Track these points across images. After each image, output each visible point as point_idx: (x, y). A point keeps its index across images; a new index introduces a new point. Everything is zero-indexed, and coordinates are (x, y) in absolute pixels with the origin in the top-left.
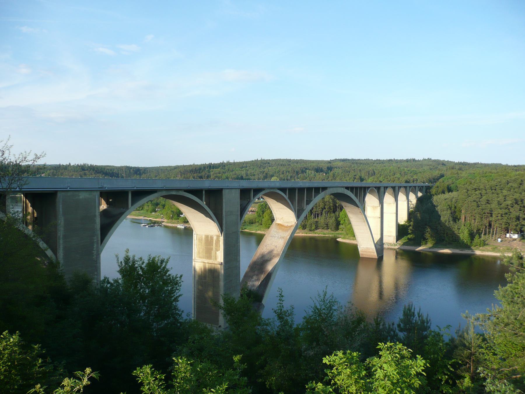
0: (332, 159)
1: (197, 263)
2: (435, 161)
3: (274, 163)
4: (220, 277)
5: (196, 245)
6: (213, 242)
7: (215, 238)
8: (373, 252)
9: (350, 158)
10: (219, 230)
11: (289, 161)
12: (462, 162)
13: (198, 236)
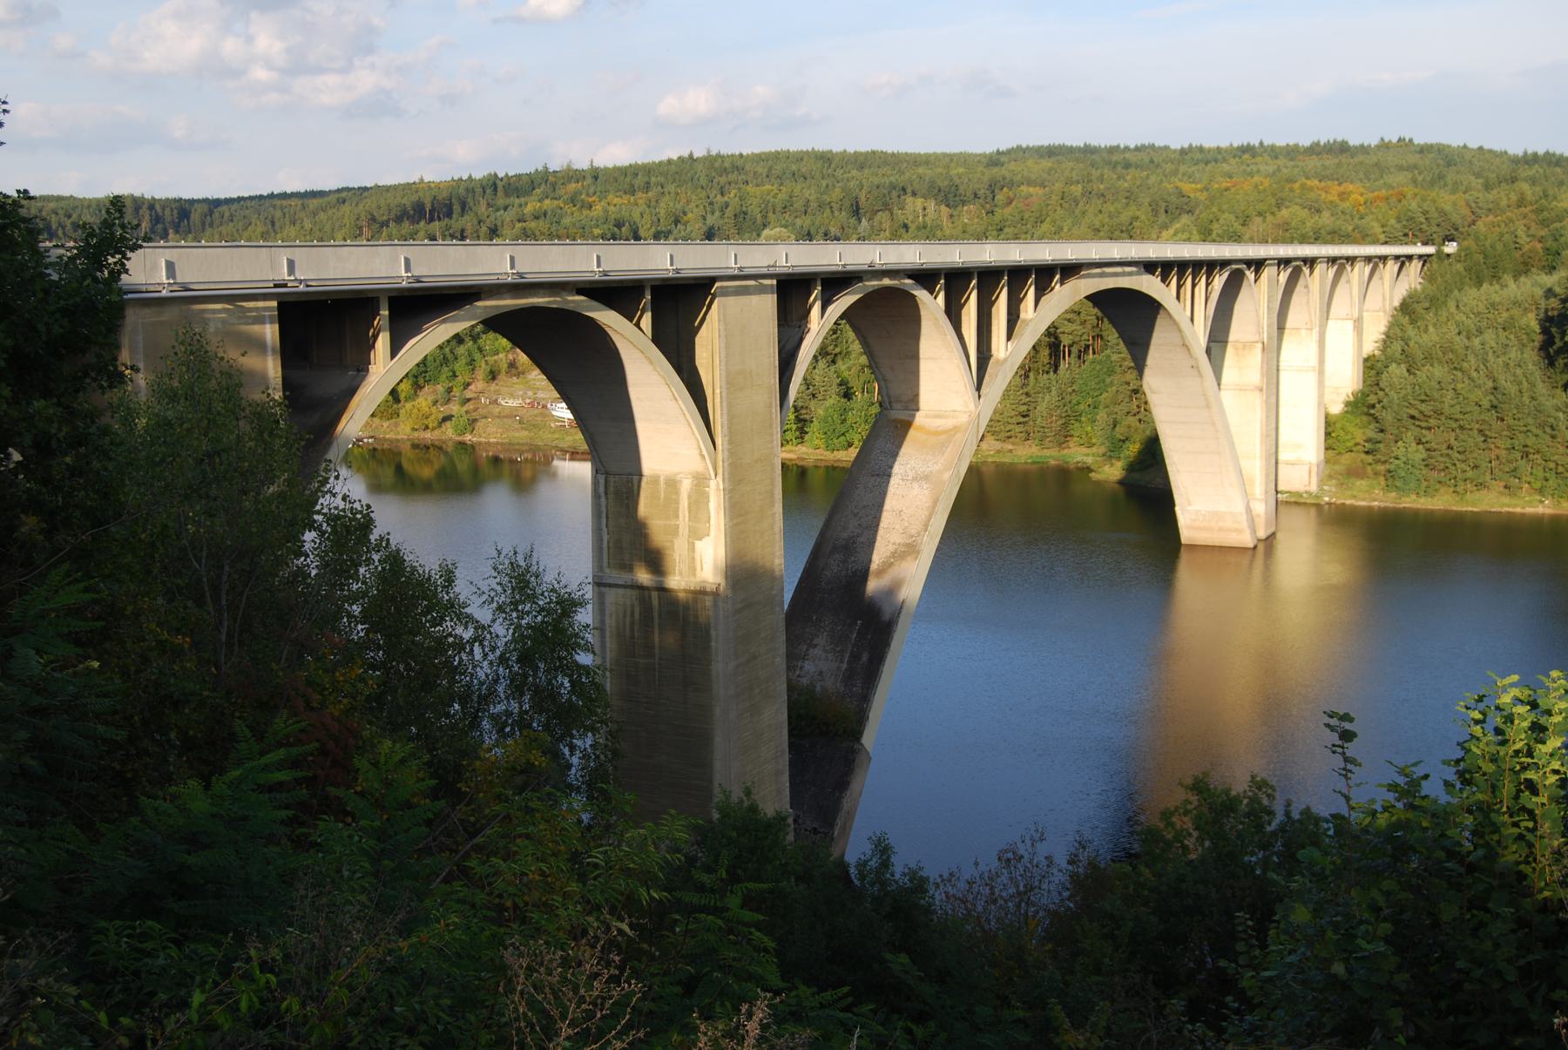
0: (1003, 148)
1: (614, 591)
2: (1424, 150)
3: (762, 169)
4: (713, 644)
5: (604, 515)
6: (677, 502)
7: (686, 485)
8: (1239, 531)
9: (1077, 141)
10: (705, 453)
11: (825, 158)
12: (1541, 152)
13: (612, 479)
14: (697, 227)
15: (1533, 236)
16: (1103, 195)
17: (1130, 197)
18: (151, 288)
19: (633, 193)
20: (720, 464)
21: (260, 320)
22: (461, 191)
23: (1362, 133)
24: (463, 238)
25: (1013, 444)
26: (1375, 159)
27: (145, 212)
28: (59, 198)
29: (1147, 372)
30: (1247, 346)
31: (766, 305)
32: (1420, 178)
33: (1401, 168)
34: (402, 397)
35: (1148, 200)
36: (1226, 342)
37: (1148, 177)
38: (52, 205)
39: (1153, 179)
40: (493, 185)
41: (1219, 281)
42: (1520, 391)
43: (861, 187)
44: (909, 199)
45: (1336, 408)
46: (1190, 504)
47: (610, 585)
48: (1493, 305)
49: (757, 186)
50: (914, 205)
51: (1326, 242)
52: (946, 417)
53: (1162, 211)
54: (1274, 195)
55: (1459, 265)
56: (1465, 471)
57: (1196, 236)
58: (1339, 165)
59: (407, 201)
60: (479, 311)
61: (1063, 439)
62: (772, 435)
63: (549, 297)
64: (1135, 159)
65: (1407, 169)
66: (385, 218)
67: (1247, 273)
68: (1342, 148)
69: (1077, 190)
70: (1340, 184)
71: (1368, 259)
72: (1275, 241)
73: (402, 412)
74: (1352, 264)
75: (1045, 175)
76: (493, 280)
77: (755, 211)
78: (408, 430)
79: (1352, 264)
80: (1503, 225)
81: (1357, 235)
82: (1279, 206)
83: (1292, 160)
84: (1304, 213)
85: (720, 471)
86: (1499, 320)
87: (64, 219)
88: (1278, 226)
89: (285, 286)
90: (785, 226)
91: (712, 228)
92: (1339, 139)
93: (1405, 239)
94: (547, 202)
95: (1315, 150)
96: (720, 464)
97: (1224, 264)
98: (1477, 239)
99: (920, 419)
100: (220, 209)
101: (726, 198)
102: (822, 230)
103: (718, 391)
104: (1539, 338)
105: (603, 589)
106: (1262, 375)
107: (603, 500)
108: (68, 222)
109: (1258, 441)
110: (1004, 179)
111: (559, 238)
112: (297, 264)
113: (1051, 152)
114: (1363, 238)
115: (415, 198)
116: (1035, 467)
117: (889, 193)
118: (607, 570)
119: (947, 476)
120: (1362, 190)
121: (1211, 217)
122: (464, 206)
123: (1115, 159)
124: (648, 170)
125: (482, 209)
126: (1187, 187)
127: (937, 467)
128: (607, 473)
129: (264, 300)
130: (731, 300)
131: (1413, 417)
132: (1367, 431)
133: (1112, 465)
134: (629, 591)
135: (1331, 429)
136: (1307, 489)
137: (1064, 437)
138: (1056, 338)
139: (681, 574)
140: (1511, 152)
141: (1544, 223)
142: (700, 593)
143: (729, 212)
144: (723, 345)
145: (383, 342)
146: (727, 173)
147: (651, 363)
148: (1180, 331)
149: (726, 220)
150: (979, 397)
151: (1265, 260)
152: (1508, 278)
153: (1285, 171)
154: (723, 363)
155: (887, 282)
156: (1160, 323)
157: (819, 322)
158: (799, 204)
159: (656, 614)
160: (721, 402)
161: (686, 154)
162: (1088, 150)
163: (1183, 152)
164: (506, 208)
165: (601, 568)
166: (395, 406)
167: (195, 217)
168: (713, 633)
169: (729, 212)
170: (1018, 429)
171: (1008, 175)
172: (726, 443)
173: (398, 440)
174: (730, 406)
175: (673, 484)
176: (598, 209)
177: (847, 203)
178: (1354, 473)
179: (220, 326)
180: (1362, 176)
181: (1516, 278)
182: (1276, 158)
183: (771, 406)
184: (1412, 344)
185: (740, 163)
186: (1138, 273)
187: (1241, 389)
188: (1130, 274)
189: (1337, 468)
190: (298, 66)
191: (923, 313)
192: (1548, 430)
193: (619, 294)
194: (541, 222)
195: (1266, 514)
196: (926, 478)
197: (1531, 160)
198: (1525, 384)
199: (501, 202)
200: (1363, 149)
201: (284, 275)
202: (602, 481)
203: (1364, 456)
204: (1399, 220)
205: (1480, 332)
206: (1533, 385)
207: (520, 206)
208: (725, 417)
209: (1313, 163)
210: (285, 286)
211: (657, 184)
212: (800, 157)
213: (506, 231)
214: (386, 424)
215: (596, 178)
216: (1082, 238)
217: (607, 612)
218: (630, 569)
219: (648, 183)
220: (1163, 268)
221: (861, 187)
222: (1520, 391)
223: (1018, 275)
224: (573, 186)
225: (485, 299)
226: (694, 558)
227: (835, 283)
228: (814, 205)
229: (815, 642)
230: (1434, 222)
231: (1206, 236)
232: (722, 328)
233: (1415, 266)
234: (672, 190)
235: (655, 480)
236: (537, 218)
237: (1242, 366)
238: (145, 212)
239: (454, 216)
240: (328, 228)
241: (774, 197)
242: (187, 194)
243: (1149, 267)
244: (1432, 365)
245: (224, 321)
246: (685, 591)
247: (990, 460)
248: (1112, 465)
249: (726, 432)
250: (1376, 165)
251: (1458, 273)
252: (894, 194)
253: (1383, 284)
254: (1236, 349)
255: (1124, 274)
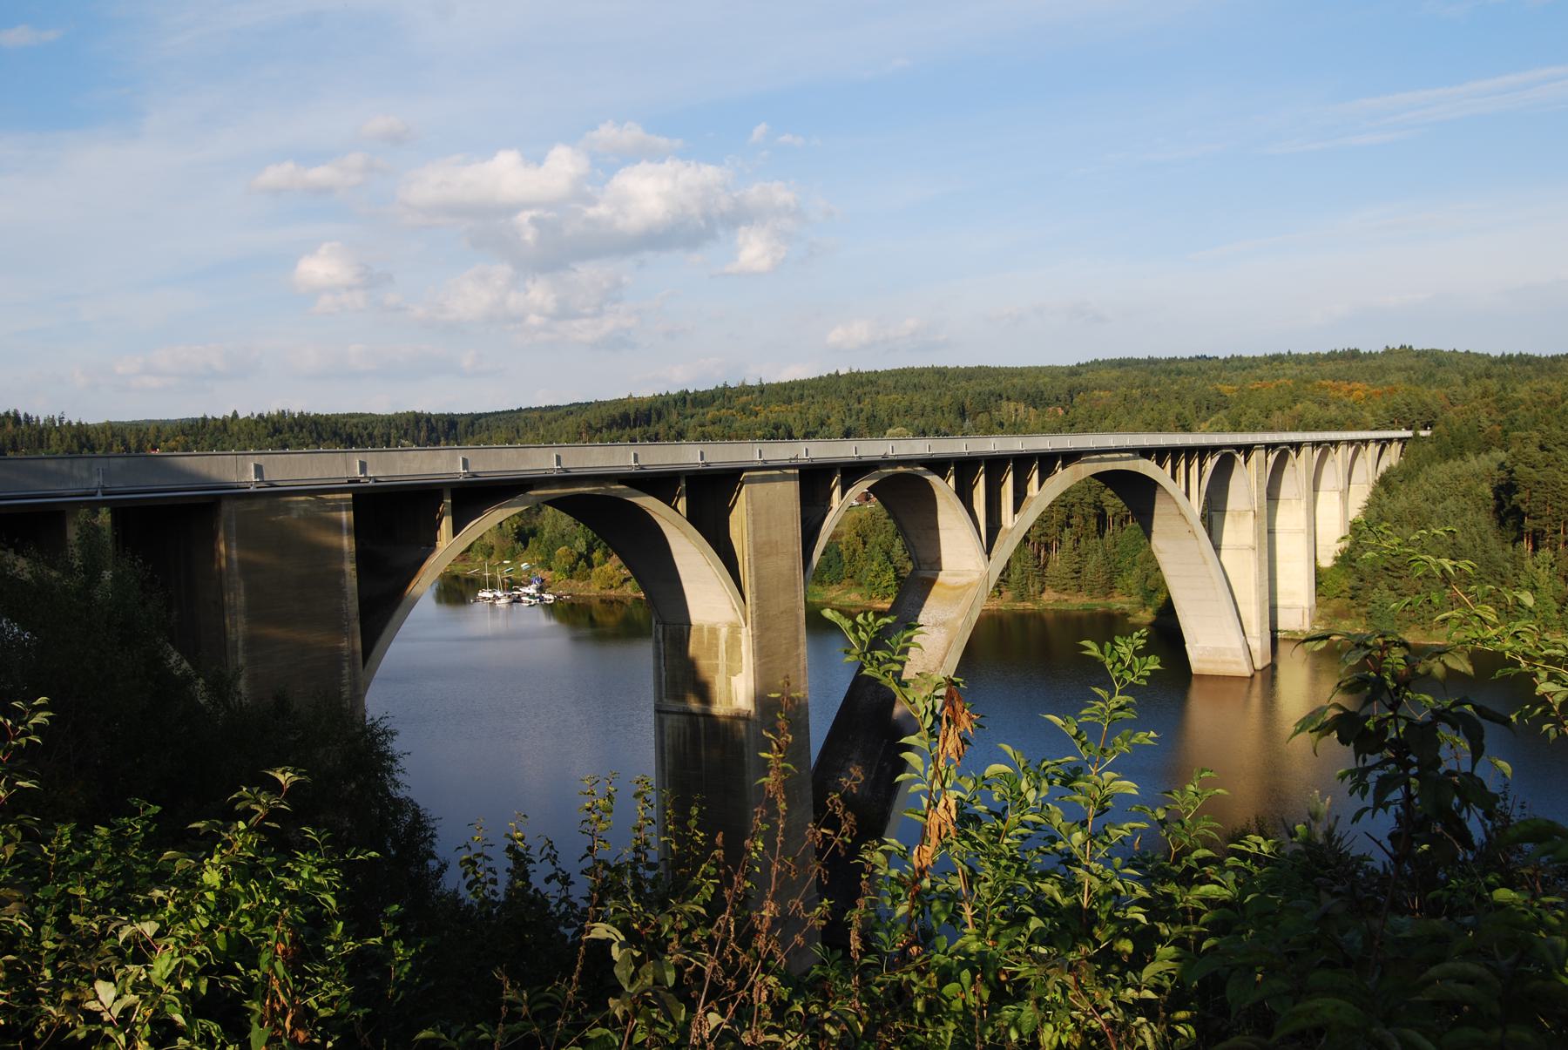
2: (1421, 354)
4: (746, 759)
6: (717, 647)
7: (724, 633)
8: (1237, 663)
10: (736, 606)
11: (941, 373)
12: (1515, 354)
14: (838, 428)
15: (1493, 421)
16: (1157, 396)
17: (1179, 397)
18: (241, 485)
19: (790, 403)
20: (749, 615)
21: (338, 508)
22: (659, 404)
23: (1371, 342)
24: (657, 439)
25: (1068, 594)
26: (1379, 362)
27: (423, 424)
28: (362, 415)
29: (1154, 536)
30: (1242, 514)
31: (788, 493)
32: (1415, 377)
33: (1399, 369)
34: (595, 563)
35: (1193, 399)
36: (1225, 511)
37: (1195, 381)
38: (355, 421)
39: (1199, 383)
40: (683, 399)
41: (1210, 464)
42: (1474, 546)
43: (967, 394)
44: (1004, 403)
45: (1326, 562)
46: (1197, 642)
47: (667, 712)
48: (1455, 477)
49: (887, 395)
50: (1008, 407)
51: (1325, 430)
52: (962, 575)
53: (1205, 408)
54: (1291, 393)
55: (1430, 445)
56: (1430, 612)
57: (1227, 427)
58: (1350, 368)
59: (616, 413)
60: (531, 499)
61: (1108, 591)
62: (796, 591)
63: (561, 488)
64: (1186, 367)
65: (1405, 370)
66: (599, 426)
67: (1237, 456)
68: (1354, 355)
69: (1137, 393)
70: (1349, 384)
71: (1351, 442)
72: (1292, 430)
73: (593, 575)
74: (1336, 447)
75: (1114, 382)
76: (541, 474)
77: (883, 415)
78: (597, 589)
79: (1336, 447)
80: (1469, 412)
81: (1349, 423)
82: (1295, 402)
83: (1313, 365)
84: (1315, 408)
85: (749, 621)
86: (1460, 489)
87: (361, 431)
88: (1294, 418)
89: (358, 482)
90: (905, 426)
91: (849, 429)
92: (1352, 348)
93: (1391, 425)
94: (724, 411)
95: (1332, 356)
96: (749, 615)
97: (1214, 449)
98: (1446, 423)
99: (942, 577)
100: (480, 421)
101: (861, 406)
102: (933, 429)
103: (746, 558)
104: (1493, 504)
105: (662, 715)
106: (1254, 537)
107: (662, 644)
108: (365, 433)
109: (1253, 591)
110: (1081, 385)
111: (730, 438)
112: (368, 466)
113: (1121, 364)
114: (1355, 426)
115: (622, 410)
116: (1086, 613)
117: (989, 398)
118: (665, 700)
119: (960, 622)
120: (1367, 387)
121: (1240, 411)
122: (660, 415)
123: (1172, 368)
124: (802, 385)
125: (674, 417)
126: (1225, 389)
127: (953, 615)
128: (664, 624)
129: (342, 493)
130: (757, 486)
131: (1387, 569)
132: (1350, 580)
133: (1145, 610)
134: (681, 717)
135: (1320, 578)
136: (1302, 628)
137: (1109, 588)
138: (1103, 510)
139: (720, 702)
140: (1493, 355)
141: (1503, 410)
142: (737, 717)
143: (863, 416)
144: (750, 522)
145: (446, 525)
146: (863, 387)
147: (686, 536)
148: (1176, 503)
149: (861, 422)
150: (989, 559)
151: (1254, 445)
152: (1471, 456)
153: (1306, 373)
154: (751, 536)
155: (901, 469)
156: (1159, 498)
157: (842, 504)
158: (917, 409)
159: (702, 736)
160: (749, 567)
161: (833, 372)
162: (1152, 361)
163: (1226, 360)
164: (692, 417)
165: (660, 699)
166: (589, 570)
167: (461, 428)
168: (746, 750)
169: (863, 416)
170: (1072, 583)
171: (1083, 382)
172: (754, 599)
173: (590, 597)
174: (757, 568)
175: (713, 631)
176: (761, 417)
177: (955, 407)
178: (1340, 614)
179: (302, 513)
180: (1368, 377)
181: (1477, 455)
182: (1300, 364)
183: (795, 569)
184: (1386, 509)
185: (874, 378)
186: (1134, 458)
187: (1239, 548)
188: (1127, 459)
189: (1326, 610)
190: (564, 313)
191: (937, 493)
192: (1498, 577)
193: (661, 484)
194: (716, 427)
195: (1262, 649)
196: (944, 624)
197: (1507, 360)
198: (1478, 540)
199: (688, 412)
200: (1371, 355)
201: (357, 473)
202: (661, 630)
203: (1349, 600)
204: (1387, 410)
205: (1444, 498)
206: (1484, 541)
207: (703, 414)
208: (753, 578)
209: (1329, 367)
210: (358, 482)
211: (809, 395)
212: (922, 372)
213: (690, 434)
214: (581, 585)
215: (762, 392)
216: (1135, 431)
217: (666, 734)
218: (683, 699)
219: (802, 395)
220: (1158, 454)
221: (967, 394)
222: (1474, 546)
223: (1022, 464)
224: (744, 399)
225: (537, 489)
226: (730, 691)
227: (852, 472)
228: (929, 409)
229: (851, 756)
230: (1415, 412)
231: (1236, 427)
232: (749, 508)
233: (1395, 449)
234: (821, 400)
235: (701, 629)
236: (714, 423)
237: (1239, 530)
238: (423, 424)
239: (652, 423)
240: (557, 434)
241: (899, 404)
242: (457, 410)
243: (1145, 453)
244: (1402, 527)
245: (306, 510)
246: (724, 716)
247: (1049, 608)
248: (1145, 610)
249: (754, 589)
250: (1380, 367)
251: (1429, 452)
252: (992, 399)
253: (1366, 462)
254: (1233, 516)
255: (1121, 459)
